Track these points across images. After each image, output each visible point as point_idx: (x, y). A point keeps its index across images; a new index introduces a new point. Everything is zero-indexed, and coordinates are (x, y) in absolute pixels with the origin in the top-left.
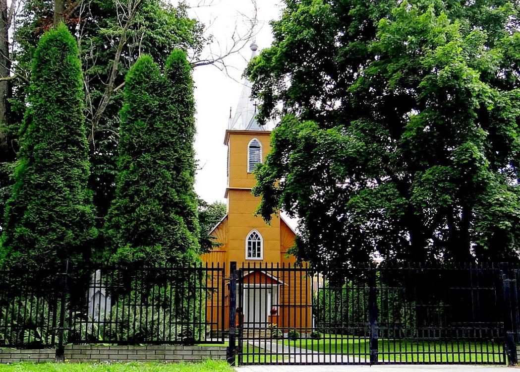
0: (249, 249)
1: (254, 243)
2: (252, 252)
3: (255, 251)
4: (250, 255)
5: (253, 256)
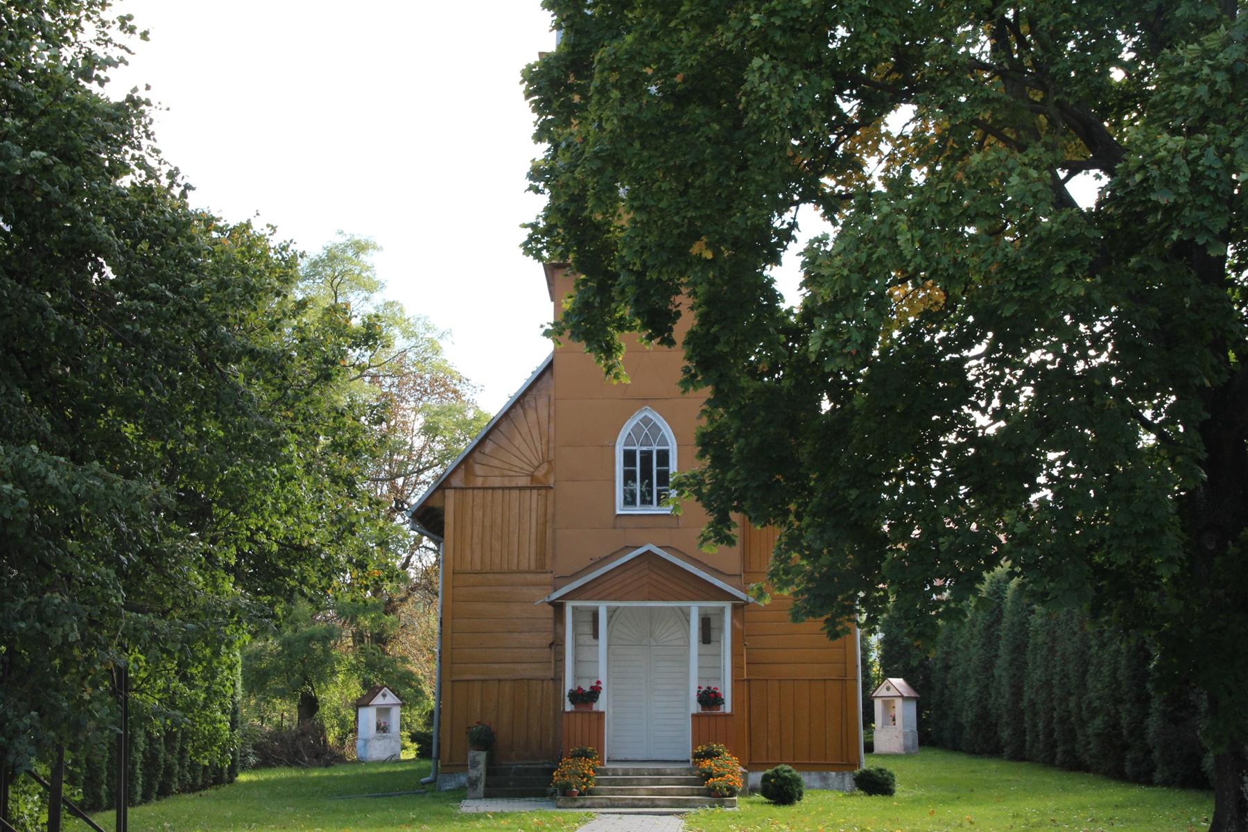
0: (629, 477)
1: (647, 457)
2: (638, 487)
3: (650, 485)
4: (630, 500)
5: (643, 502)
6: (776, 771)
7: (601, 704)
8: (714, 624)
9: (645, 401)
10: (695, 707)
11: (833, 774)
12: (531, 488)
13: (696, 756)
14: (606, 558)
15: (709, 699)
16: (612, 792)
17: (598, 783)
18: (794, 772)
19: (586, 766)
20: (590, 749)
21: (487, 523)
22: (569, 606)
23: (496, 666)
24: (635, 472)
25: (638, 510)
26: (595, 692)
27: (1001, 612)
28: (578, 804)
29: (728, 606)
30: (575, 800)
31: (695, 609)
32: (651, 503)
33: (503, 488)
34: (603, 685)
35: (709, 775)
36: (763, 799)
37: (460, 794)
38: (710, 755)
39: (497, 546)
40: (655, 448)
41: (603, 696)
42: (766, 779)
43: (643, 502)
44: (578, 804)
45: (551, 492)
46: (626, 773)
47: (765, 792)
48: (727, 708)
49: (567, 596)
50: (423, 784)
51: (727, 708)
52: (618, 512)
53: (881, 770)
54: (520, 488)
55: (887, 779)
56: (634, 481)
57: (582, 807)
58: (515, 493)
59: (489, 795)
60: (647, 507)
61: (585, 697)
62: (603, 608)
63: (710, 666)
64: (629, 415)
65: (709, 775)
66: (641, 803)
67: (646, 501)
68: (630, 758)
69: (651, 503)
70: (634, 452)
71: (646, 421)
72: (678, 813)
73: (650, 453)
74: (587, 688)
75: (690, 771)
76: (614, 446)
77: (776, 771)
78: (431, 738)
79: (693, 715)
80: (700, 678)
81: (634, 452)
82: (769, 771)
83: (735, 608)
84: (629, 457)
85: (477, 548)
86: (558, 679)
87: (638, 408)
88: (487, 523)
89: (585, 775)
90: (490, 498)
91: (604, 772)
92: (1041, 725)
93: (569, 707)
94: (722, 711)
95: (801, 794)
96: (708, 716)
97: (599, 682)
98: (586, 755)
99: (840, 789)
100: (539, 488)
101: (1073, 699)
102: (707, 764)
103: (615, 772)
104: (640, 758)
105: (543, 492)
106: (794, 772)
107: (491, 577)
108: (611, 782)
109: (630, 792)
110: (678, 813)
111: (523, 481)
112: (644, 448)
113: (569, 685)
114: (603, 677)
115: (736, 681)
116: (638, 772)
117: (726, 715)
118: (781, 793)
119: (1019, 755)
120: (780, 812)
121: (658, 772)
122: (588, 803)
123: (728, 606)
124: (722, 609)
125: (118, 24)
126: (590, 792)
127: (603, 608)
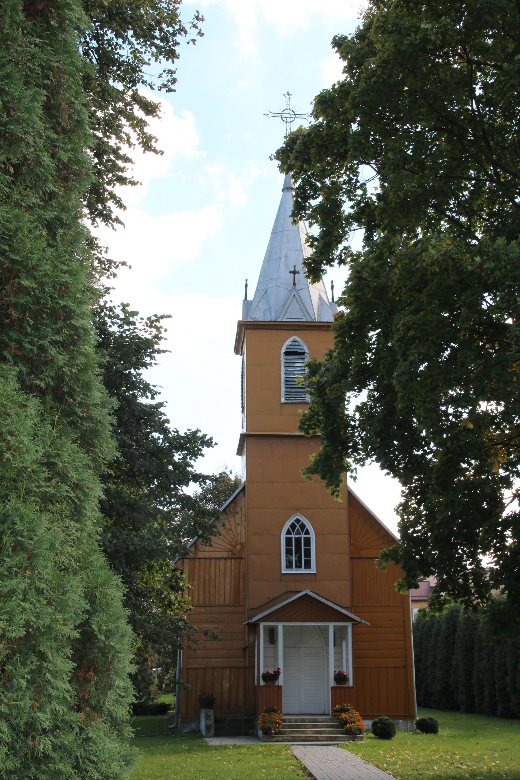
0: (289, 552)
1: (298, 541)
2: (294, 558)
3: (300, 557)
4: (289, 565)
5: (296, 566)
6: (381, 720)
7: (281, 681)
8: (268, 639)
9: (297, 510)
10: (332, 683)
11: (401, 721)
12: (231, 559)
13: (334, 711)
14: (276, 598)
15: (340, 678)
16: (292, 732)
17: (284, 727)
18: (390, 720)
19: (276, 717)
20: (275, 707)
21: (207, 577)
22: (262, 625)
23: (214, 660)
24: (292, 549)
25: (294, 571)
26: (277, 674)
27: (455, 630)
28: (274, 740)
29: (349, 625)
30: (273, 737)
31: (331, 626)
32: (300, 566)
33: (216, 559)
34: (281, 671)
35: (346, 723)
36: (373, 736)
37: (196, 734)
38: (344, 710)
39: (212, 591)
40: (303, 536)
41: (281, 677)
42: (374, 724)
43: (296, 566)
44: (274, 740)
45: (243, 562)
46: (296, 721)
47: (374, 732)
48: (351, 683)
49: (263, 619)
50: (170, 729)
51: (351, 683)
52: (283, 572)
53: (431, 719)
54: (225, 559)
55: (434, 724)
56: (292, 555)
57: (282, 741)
58: (222, 562)
59: (217, 735)
60: (298, 569)
61: (271, 678)
62: (280, 626)
63: (338, 660)
64: (288, 518)
65: (346, 723)
66: (310, 739)
67: (298, 566)
68: (290, 712)
69: (300, 566)
70: (292, 538)
71: (298, 521)
72: (334, 745)
73: (300, 539)
74: (271, 672)
75: (332, 720)
76: (280, 535)
77: (381, 720)
78: (419, 705)
79: (332, 688)
80: (335, 667)
81: (292, 538)
82: (376, 720)
83: (353, 625)
84: (289, 541)
85: (201, 592)
86: (251, 666)
87: (294, 514)
88: (207, 577)
89: (277, 723)
90: (208, 564)
91: (284, 721)
92: (486, 693)
93: (262, 683)
94: (347, 685)
95: (395, 733)
96: (341, 688)
97: (279, 669)
98: (275, 711)
99: (407, 730)
100: (235, 559)
101: (508, 679)
102: (344, 715)
103: (290, 721)
104: (296, 712)
105: (238, 560)
106: (390, 720)
107: (208, 609)
108: (290, 727)
109: (302, 732)
110: (334, 745)
111: (225, 555)
112: (297, 536)
113: (262, 671)
114: (281, 665)
115: (354, 668)
116: (303, 721)
117: (350, 688)
118: (384, 732)
119: (471, 709)
120: (386, 743)
121: (314, 721)
122: (280, 739)
123: (349, 625)
124: (346, 627)
125: (121, 307)
126: (280, 733)
127: (280, 626)
